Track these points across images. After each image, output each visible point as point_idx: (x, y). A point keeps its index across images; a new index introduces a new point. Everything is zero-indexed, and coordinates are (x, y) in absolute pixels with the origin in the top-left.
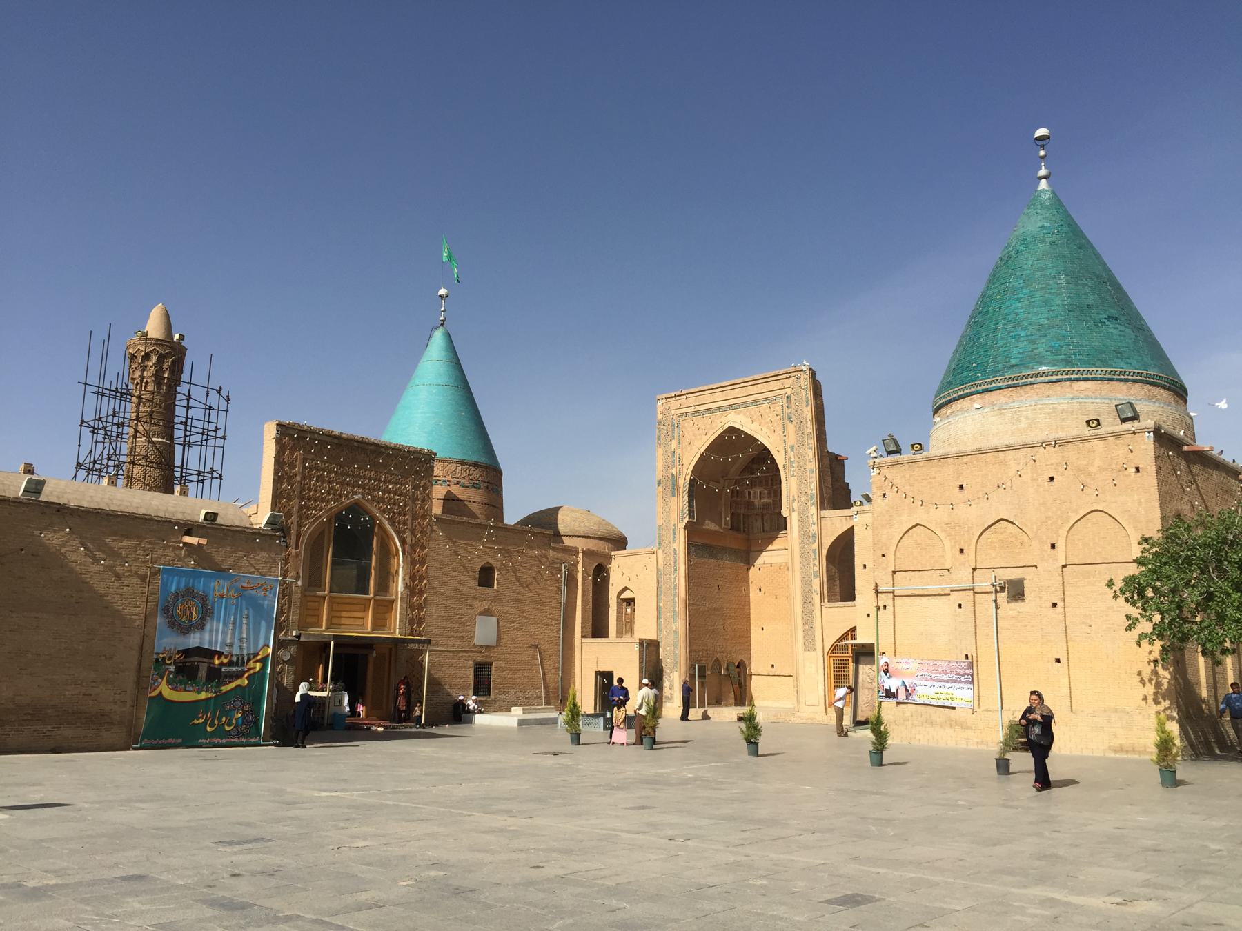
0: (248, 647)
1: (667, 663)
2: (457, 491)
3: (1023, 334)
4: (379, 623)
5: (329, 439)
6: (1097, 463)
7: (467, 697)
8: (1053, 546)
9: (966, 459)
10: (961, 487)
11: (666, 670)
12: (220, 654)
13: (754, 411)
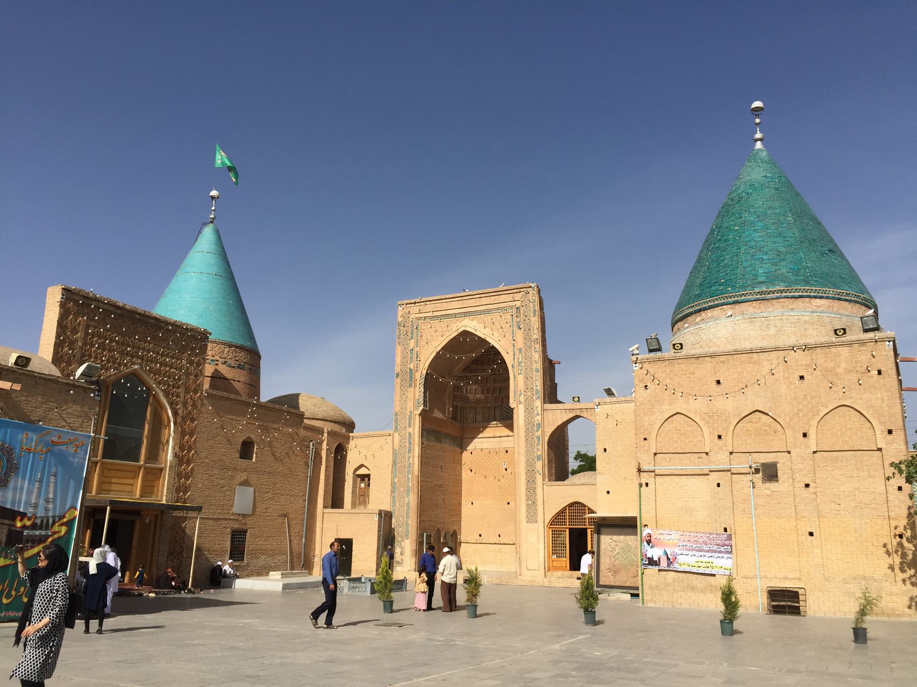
0: (54, 509)
1: (399, 532)
2: (223, 369)
3: (765, 257)
4: (148, 488)
5: (113, 309)
6: (843, 365)
7: (224, 564)
8: (805, 435)
9: (722, 358)
10: (718, 382)
11: (398, 538)
12: (23, 515)
13: (487, 318)
